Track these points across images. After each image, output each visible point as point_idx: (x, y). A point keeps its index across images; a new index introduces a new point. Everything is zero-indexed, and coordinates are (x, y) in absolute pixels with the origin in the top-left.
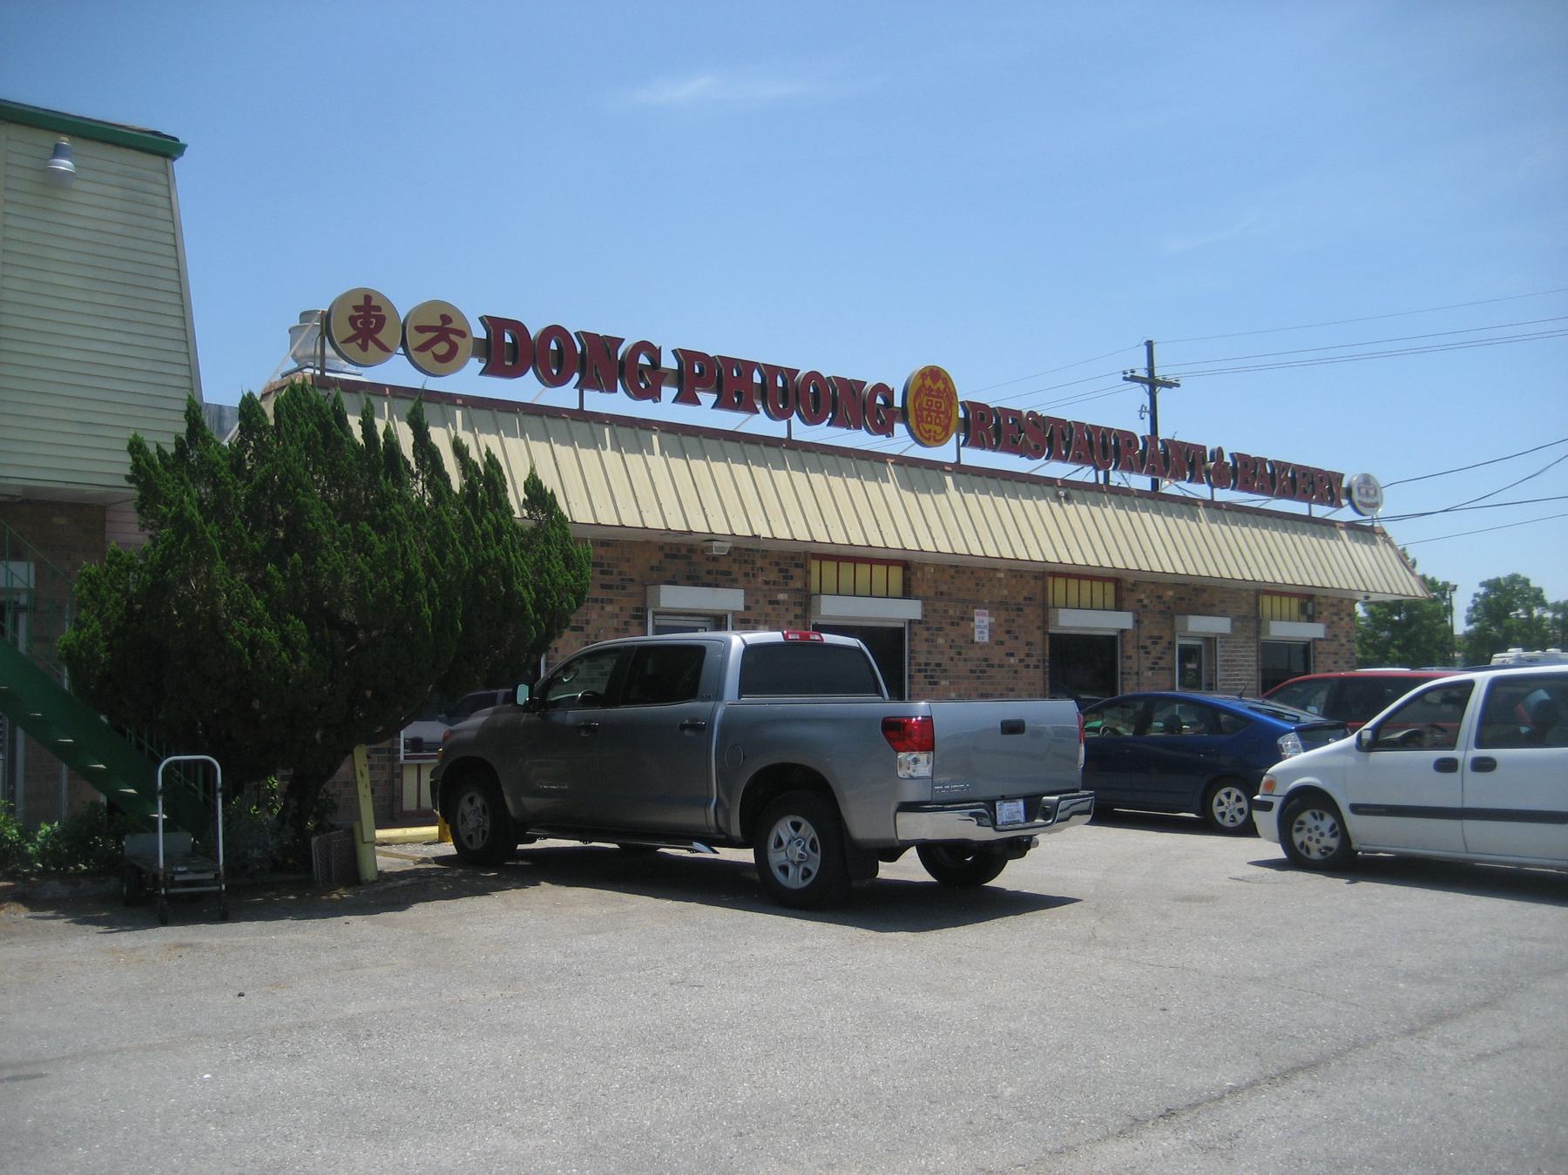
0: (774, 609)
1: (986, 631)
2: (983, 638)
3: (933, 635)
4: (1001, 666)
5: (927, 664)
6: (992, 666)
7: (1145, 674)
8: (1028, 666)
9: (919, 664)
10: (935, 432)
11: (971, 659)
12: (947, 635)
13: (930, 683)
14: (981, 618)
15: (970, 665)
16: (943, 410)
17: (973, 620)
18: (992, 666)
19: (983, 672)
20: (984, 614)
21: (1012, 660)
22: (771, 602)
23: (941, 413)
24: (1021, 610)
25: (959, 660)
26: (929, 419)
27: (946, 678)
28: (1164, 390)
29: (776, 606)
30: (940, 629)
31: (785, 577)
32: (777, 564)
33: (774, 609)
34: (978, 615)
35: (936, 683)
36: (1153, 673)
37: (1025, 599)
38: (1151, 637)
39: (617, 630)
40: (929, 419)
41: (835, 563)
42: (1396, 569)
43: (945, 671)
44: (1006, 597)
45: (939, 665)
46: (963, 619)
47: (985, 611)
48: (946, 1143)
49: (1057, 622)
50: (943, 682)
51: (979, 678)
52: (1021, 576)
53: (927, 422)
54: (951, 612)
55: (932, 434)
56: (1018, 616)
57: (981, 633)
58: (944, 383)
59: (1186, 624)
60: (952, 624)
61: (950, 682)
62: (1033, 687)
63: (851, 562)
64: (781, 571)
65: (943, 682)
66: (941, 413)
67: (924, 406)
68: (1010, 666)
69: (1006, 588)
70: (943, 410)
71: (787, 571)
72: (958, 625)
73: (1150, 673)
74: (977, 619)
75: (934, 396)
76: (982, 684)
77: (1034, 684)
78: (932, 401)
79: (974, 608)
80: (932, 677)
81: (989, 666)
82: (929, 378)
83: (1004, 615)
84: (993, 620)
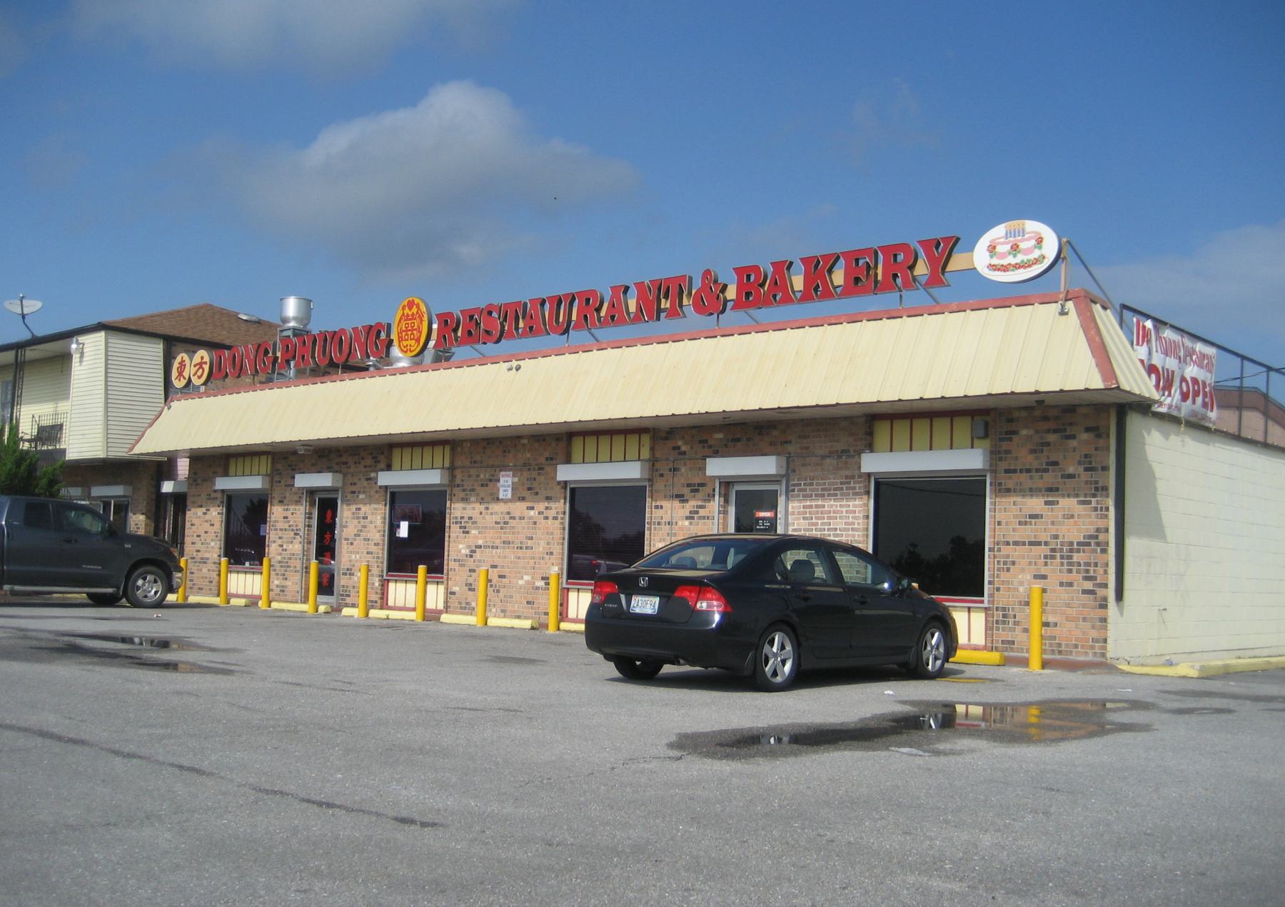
0: (368, 484)
1: (510, 489)
2: (507, 495)
3: (467, 495)
4: (522, 518)
5: (462, 518)
6: (513, 518)
7: (680, 523)
8: (546, 518)
9: (456, 518)
10: (410, 345)
11: (496, 513)
12: (478, 495)
13: (464, 532)
14: (506, 479)
15: (496, 518)
16: (416, 327)
17: (499, 481)
18: (513, 518)
19: (506, 523)
20: (508, 476)
21: (532, 513)
22: (367, 479)
23: (415, 330)
24: (542, 469)
25: (487, 514)
26: (406, 337)
27: (477, 528)
28: (1231, 431)
29: (369, 481)
30: (473, 490)
31: (376, 462)
32: (372, 454)
33: (368, 484)
34: (503, 476)
35: (468, 532)
36: (691, 524)
37: (547, 459)
38: (688, 485)
39: (296, 501)
40: (406, 337)
41: (889, 422)
42: (1136, 381)
43: (475, 523)
44: (529, 459)
45: (470, 518)
46: (491, 480)
47: (509, 473)
48: (567, 873)
49: (642, 468)
50: (473, 532)
51: (502, 528)
52: (544, 440)
53: (406, 340)
54: (482, 476)
55: (408, 347)
56: (539, 474)
57: (505, 491)
58: (417, 307)
59: (779, 466)
60: (482, 485)
61: (479, 532)
62: (551, 536)
63: (907, 418)
64: (373, 458)
65: (473, 532)
66: (415, 330)
67: (404, 329)
68: (530, 518)
69: (529, 452)
70: (416, 327)
71: (376, 458)
72: (487, 485)
73: (687, 523)
74: (502, 480)
75: (410, 320)
76: (505, 533)
77: (552, 533)
78: (408, 324)
79: (501, 471)
80: (465, 527)
81: (511, 518)
82: (407, 308)
83: (526, 474)
84: (516, 480)
